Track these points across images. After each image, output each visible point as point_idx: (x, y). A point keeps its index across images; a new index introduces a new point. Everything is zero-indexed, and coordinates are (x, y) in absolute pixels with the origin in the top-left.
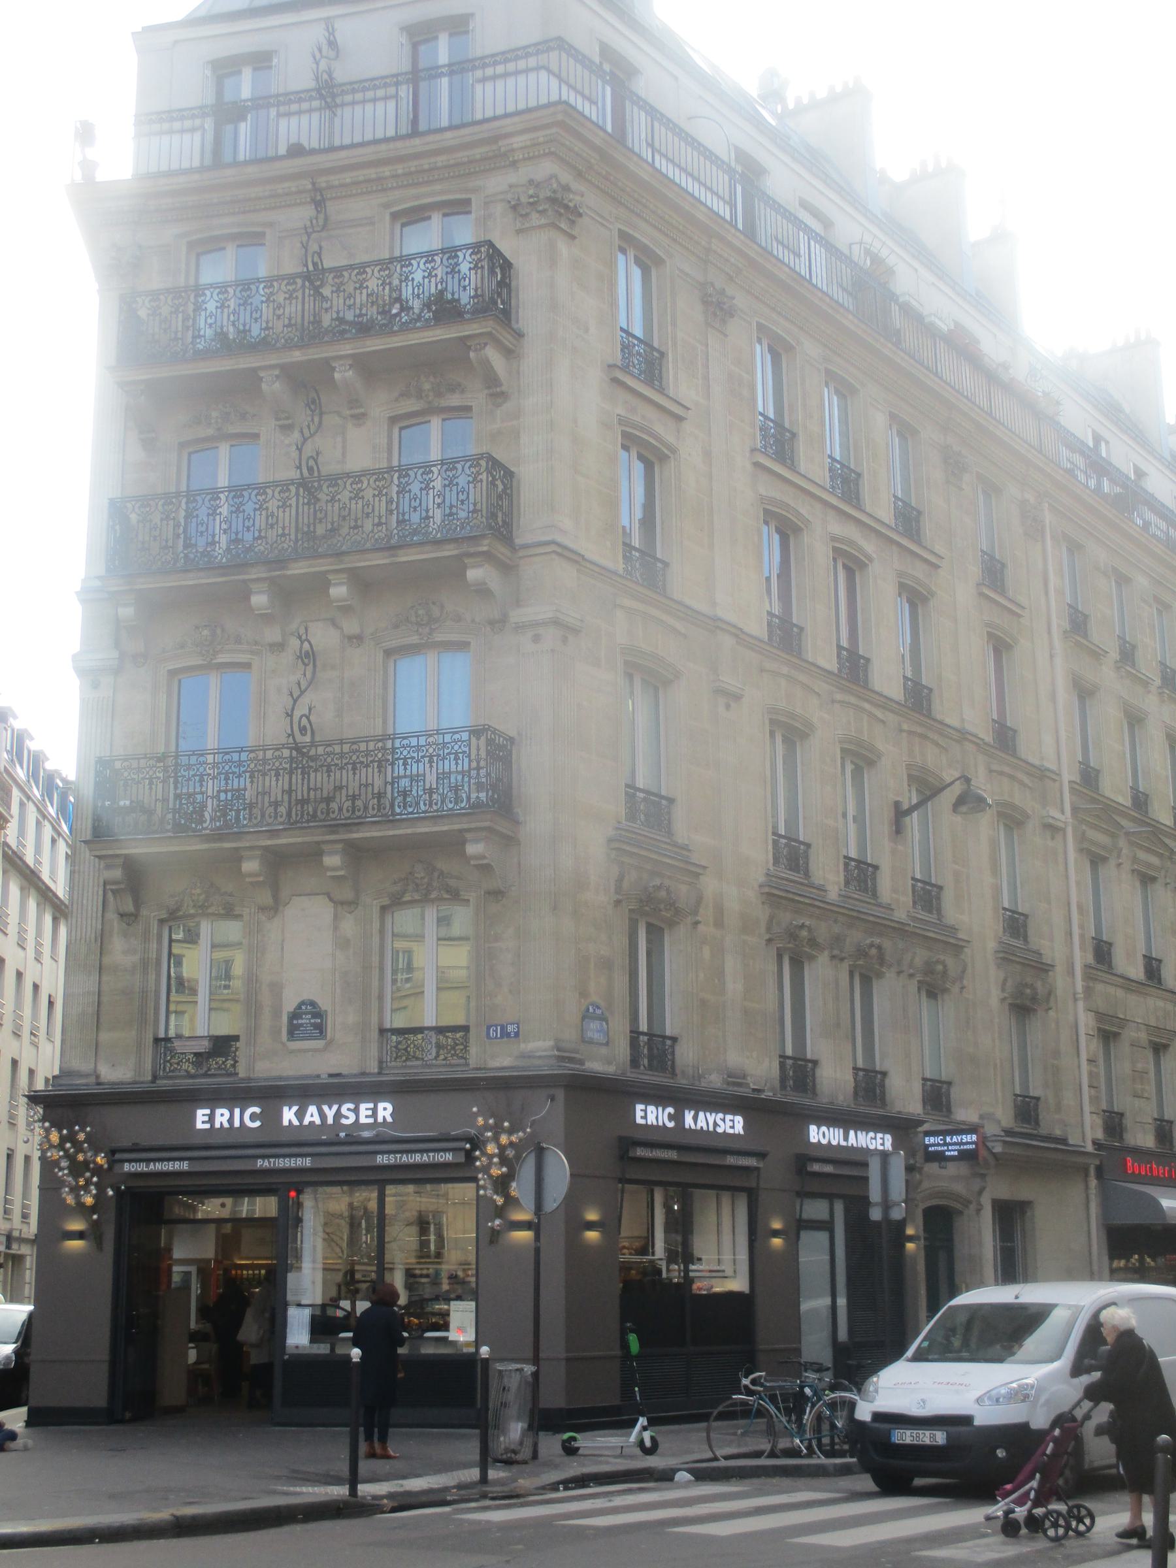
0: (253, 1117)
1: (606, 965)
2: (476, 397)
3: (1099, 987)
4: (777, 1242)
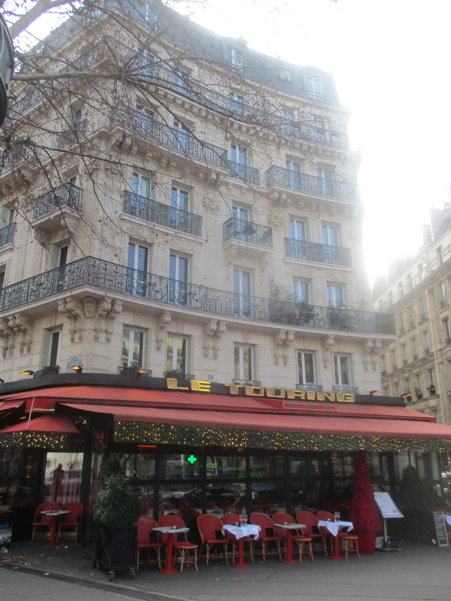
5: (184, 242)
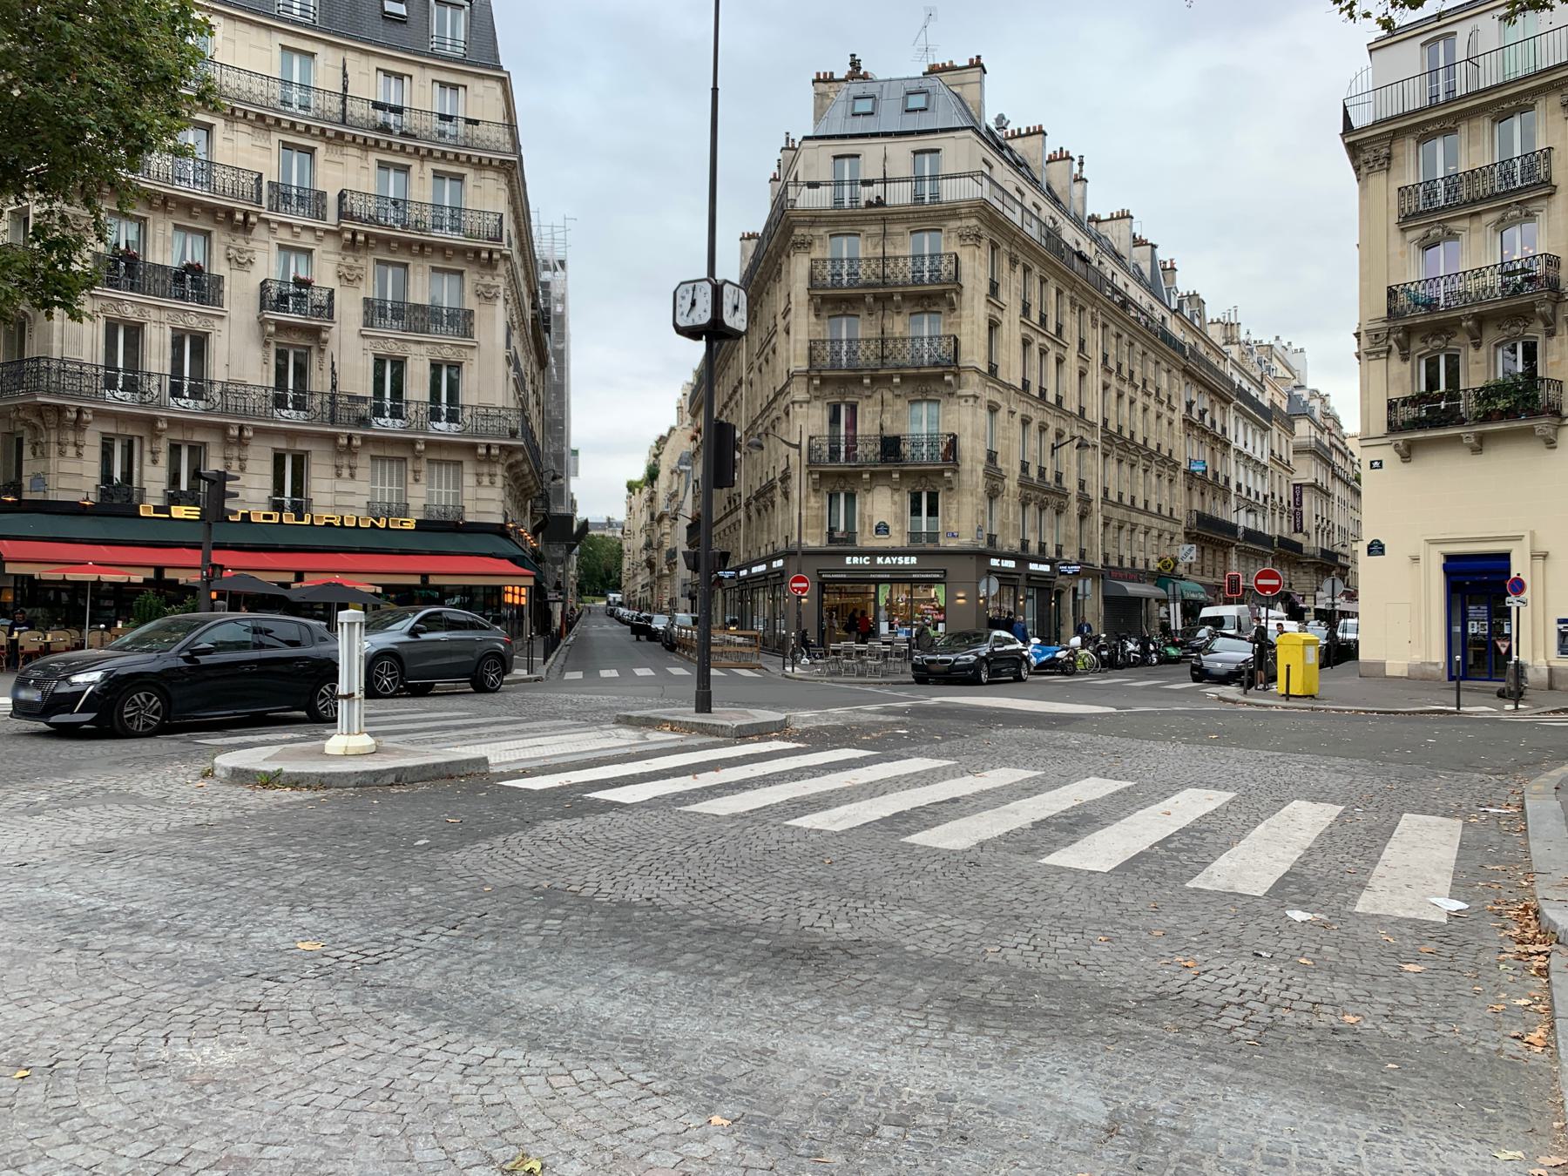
2: (945, 309)
5: (193, 317)
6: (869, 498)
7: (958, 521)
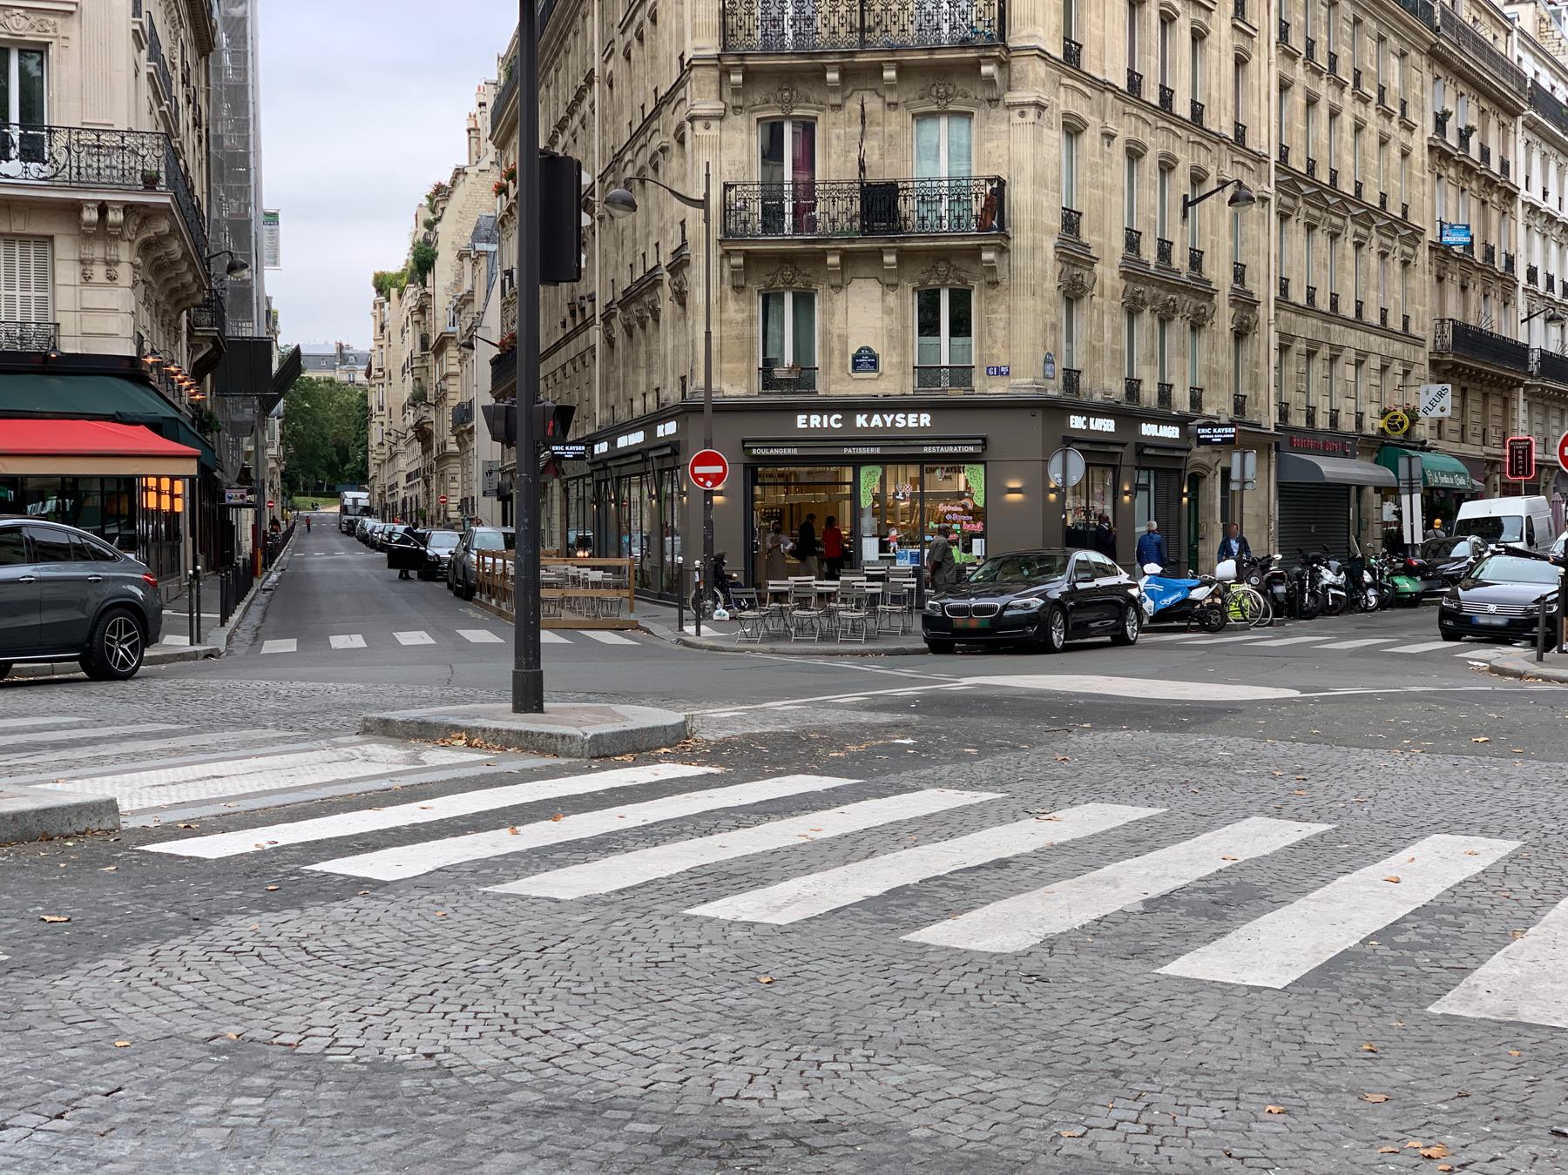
0: (837, 421)
1: (1054, 327)
3: (1282, 313)
4: (1127, 498)
6: (839, 300)
7: (1008, 346)
